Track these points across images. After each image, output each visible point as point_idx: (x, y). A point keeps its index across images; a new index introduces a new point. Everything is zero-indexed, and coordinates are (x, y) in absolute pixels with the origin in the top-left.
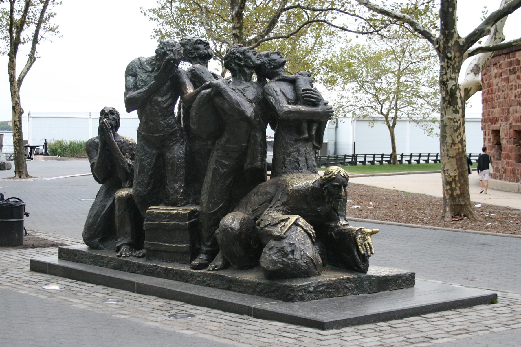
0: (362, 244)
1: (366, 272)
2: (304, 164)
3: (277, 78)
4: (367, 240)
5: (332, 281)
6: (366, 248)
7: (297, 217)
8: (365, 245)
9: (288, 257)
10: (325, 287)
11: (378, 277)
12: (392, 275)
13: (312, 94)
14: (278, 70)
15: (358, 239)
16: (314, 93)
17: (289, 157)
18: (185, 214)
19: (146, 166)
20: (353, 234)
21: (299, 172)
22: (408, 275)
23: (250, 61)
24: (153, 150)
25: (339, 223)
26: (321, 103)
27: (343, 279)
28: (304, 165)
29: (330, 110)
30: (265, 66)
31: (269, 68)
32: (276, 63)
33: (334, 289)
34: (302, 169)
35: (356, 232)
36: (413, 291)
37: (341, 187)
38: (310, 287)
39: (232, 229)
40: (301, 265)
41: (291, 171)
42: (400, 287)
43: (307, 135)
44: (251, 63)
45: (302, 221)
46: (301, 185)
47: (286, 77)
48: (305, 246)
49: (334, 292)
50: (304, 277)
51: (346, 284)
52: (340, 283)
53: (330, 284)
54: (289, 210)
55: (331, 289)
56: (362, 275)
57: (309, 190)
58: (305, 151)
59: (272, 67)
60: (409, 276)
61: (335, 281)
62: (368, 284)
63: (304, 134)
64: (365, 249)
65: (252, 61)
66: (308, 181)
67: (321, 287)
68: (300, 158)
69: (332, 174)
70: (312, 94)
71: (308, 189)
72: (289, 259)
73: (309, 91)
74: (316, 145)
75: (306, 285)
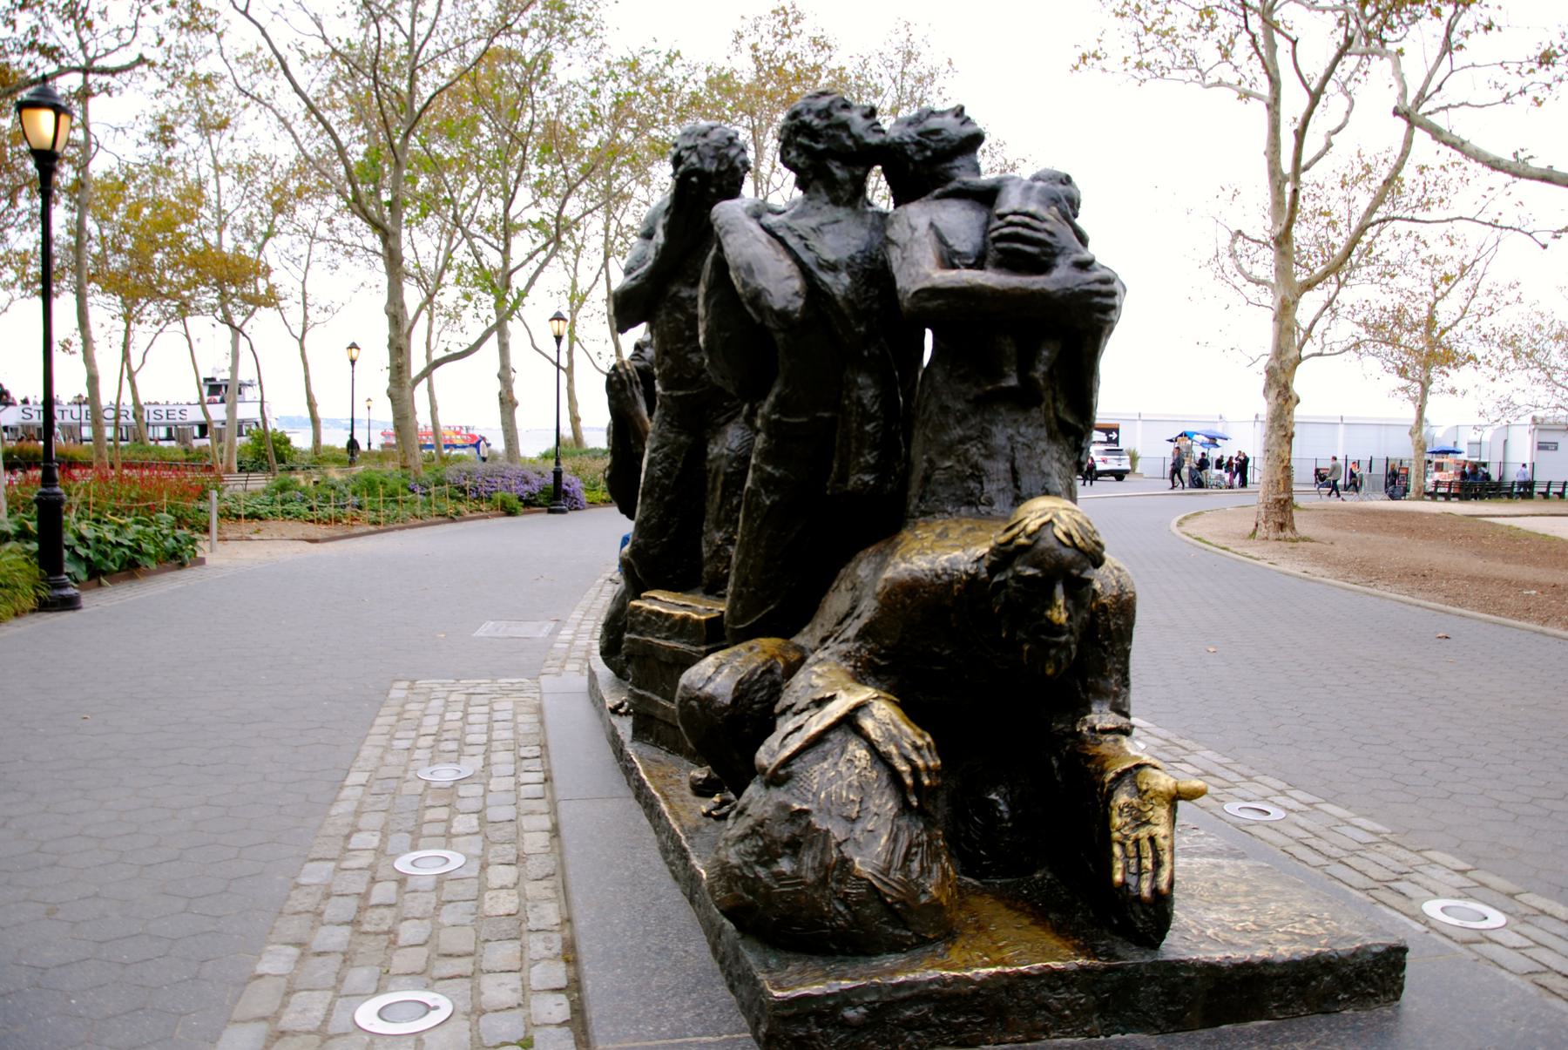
0: (1126, 837)
1: (1155, 946)
2: (1003, 484)
3: (937, 192)
4: (1148, 822)
5: (969, 980)
6: (1139, 857)
7: (866, 693)
8: (1137, 842)
9: (775, 869)
10: (932, 1005)
11: (1211, 970)
12: (1287, 956)
13: (1026, 226)
14: (948, 165)
15: (1115, 813)
16: (1035, 223)
17: (949, 458)
18: (698, 622)
19: (659, 478)
20: (1103, 784)
21: (980, 516)
22: (1369, 957)
23: (844, 135)
24: (679, 434)
25: (1085, 722)
26: (1060, 260)
27: (1023, 976)
28: (1002, 490)
29: (1104, 288)
30: (903, 151)
31: (917, 158)
32: (942, 140)
33: (981, 1014)
34: (990, 503)
35: (1113, 780)
36: (1396, 1017)
37: (1053, 588)
38: (854, 1006)
39: (710, 699)
40: (820, 909)
41: (949, 509)
42: (1324, 1004)
43: (1012, 381)
44: (849, 143)
45: (882, 717)
46: (926, 566)
47: (964, 183)
48: (858, 827)
49: (980, 1024)
50: (845, 953)
51: (1045, 993)
52: (1007, 989)
53: (957, 996)
54: (882, 657)
55: (965, 1013)
56: (1135, 957)
57: (956, 586)
58: (1010, 438)
59: (929, 153)
60: (1375, 963)
61: (984, 982)
62: (1156, 995)
63: (1004, 376)
64: (1133, 862)
65: (851, 136)
66: (958, 553)
67: (909, 1007)
68: (987, 464)
69: (1016, 530)
70: (1026, 226)
71: (951, 583)
72: (779, 876)
73: (1027, 220)
74: (1070, 420)
75: (829, 996)
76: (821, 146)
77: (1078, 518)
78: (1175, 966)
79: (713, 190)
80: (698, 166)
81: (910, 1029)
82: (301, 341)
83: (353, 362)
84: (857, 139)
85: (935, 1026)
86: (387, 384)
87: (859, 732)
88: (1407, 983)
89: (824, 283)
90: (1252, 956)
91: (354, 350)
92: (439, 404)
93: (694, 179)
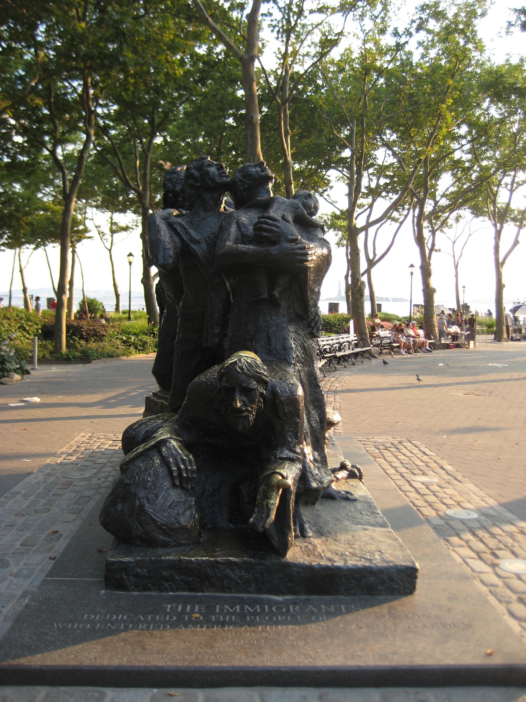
24: (41, 329)
76: (198, 184)
77: (249, 361)
78: (289, 565)
79: (180, 199)
80: (172, 188)
81: (167, 581)
82: (110, 250)
83: (130, 263)
84: (213, 180)
85: (178, 581)
86: (142, 276)
87: (160, 452)
88: (417, 586)
89: (194, 249)
90: (333, 565)
91: (131, 257)
92: (386, 257)
93: (170, 195)
